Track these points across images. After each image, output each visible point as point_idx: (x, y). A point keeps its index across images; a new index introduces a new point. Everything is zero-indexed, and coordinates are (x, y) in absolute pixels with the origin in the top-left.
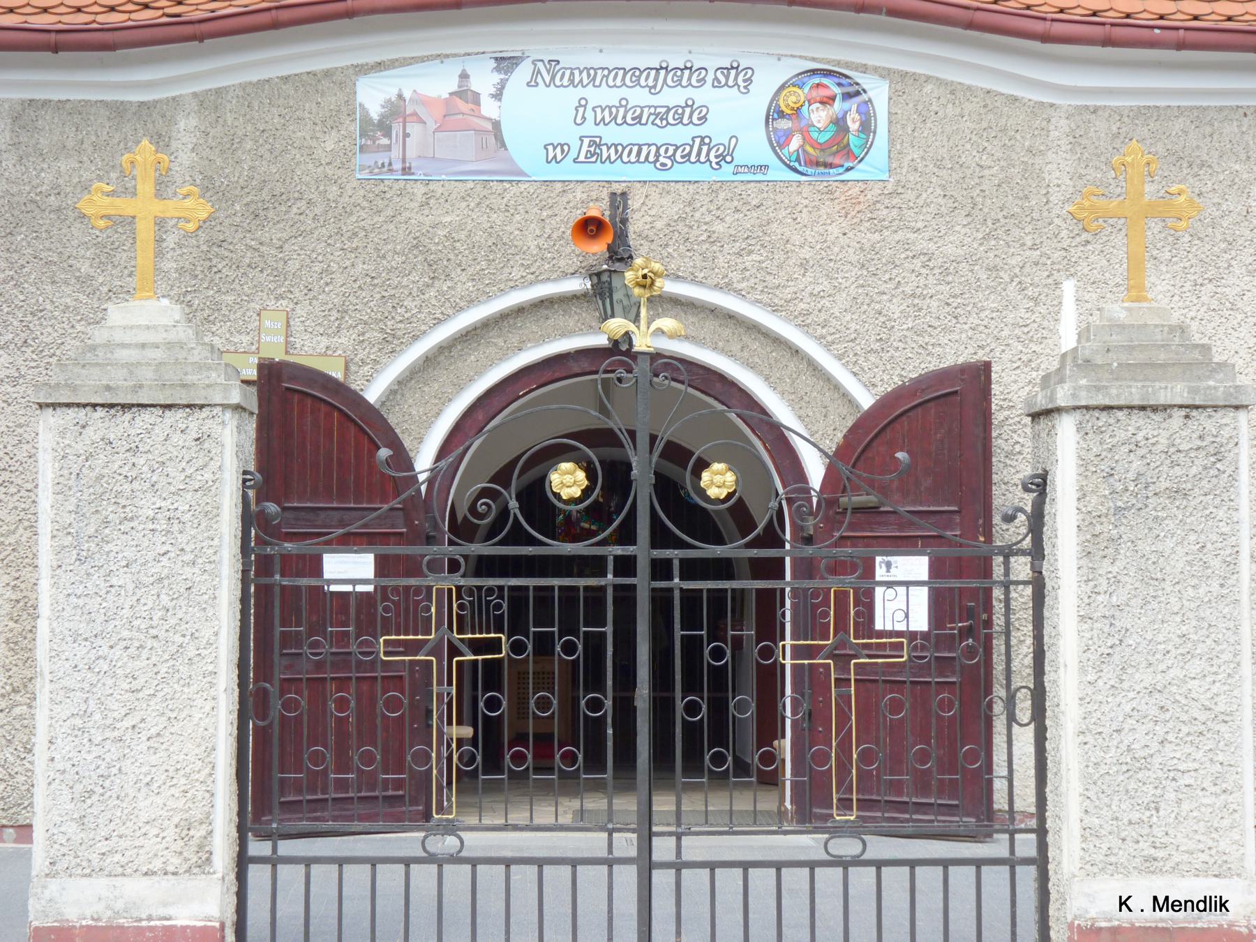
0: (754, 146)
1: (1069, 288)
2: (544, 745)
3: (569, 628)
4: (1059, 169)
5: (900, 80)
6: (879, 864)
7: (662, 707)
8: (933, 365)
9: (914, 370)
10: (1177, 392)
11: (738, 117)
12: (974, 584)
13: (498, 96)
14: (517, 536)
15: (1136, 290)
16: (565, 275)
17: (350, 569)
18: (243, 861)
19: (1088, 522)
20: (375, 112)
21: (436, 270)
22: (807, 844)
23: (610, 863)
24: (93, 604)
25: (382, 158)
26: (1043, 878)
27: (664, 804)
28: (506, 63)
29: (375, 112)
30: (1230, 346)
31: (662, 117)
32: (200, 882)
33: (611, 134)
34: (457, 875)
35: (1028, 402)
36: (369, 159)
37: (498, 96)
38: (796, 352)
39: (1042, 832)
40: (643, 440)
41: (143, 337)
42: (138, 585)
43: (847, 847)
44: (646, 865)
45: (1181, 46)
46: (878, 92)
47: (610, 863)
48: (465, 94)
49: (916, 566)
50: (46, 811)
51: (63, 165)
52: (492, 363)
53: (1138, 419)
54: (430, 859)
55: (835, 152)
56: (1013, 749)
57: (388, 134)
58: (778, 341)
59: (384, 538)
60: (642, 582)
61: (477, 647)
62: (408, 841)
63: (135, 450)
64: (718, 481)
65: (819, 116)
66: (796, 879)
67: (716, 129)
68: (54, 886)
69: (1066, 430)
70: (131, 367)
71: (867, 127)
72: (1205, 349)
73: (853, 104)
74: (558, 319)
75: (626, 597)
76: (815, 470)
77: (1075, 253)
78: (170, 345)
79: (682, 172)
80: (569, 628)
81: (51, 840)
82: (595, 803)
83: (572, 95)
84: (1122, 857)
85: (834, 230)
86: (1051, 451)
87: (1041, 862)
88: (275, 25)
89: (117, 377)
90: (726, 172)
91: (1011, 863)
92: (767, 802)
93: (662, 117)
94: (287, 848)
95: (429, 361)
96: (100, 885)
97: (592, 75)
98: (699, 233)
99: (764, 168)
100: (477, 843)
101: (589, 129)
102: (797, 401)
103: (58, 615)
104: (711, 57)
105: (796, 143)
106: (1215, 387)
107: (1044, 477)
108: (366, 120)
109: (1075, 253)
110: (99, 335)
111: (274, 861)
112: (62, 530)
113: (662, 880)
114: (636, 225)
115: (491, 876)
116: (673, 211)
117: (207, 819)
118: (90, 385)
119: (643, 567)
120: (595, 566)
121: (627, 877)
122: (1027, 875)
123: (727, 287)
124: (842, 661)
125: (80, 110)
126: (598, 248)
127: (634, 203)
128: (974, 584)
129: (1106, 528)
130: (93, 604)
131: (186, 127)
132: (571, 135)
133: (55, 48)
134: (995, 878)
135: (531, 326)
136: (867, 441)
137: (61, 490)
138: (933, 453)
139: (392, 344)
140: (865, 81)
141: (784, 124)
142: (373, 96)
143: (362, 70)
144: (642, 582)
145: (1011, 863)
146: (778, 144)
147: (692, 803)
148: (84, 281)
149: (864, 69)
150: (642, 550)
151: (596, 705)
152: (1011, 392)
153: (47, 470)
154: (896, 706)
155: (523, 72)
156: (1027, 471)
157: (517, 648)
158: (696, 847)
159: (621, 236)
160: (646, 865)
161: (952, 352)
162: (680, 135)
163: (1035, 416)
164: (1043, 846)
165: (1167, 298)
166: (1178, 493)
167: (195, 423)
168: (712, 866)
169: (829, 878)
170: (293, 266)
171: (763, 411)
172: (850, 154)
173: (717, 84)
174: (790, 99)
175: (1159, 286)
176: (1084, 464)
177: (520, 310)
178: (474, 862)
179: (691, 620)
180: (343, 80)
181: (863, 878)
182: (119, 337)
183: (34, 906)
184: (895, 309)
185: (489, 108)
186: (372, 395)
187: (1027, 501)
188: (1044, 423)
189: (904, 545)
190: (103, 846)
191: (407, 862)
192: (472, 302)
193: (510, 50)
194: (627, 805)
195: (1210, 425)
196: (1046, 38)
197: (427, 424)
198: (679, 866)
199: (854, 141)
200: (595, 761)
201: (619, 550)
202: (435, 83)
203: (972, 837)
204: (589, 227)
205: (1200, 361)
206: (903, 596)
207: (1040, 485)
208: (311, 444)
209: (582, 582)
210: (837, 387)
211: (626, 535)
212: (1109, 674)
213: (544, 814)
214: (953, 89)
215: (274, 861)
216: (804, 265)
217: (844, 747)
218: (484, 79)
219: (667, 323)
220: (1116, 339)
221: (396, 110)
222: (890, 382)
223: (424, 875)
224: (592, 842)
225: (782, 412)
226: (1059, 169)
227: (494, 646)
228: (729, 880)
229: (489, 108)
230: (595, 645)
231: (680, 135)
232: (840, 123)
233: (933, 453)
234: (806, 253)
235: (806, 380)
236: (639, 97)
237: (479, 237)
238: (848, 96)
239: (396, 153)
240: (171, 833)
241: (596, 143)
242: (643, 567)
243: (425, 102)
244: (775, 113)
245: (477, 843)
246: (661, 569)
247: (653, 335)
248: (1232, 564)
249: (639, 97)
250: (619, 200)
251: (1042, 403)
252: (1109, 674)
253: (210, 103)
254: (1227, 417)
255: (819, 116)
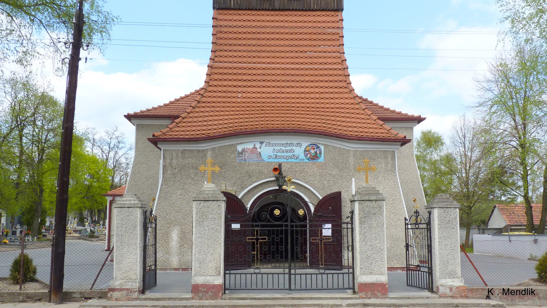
0: (302, 156)
1: (353, 179)
2: (265, 255)
3: (277, 236)
4: (351, 160)
5: (325, 146)
6: (327, 274)
7: (292, 248)
8: (332, 192)
9: (329, 192)
10: (374, 198)
11: (299, 151)
12: (339, 228)
13: (260, 148)
14: (269, 221)
15: (367, 181)
16: (271, 177)
17: (236, 226)
18: (225, 274)
19: (360, 219)
20: (240, 151)
21: (250, 177)
22: (316, 271)
23: (284, 274)
24: (202, 232)
25: (241, 158)
26: (354, 276)
27: (293, 265)
28: (261, 143)
29: (240, 151)
30: (380, 189)
31: (287, 151)
32: (219, 277)
33: (279, 154)
34: (259, 276)
35: (350, 199)
36: (239, 158)
37: (260, 148)
38: (309, 190)
39: (353, 268)
40: (289, 206)
41: (209, 189)
42: (209, 229)
43: (322, 271)
44: (290, 274)
45: (371, 141)
46: (322, 148)
47: (284, 274)
48: (255, 148)
49: (329, 226)
50: (195, 266)
51: (189, 160)
52: (259, 192)
53: (368, 202)
54: (255, 273)
55: (315, 157)
56: (346, 255)
57: (242, 154)
58: (306, 188)
59: (244, 221)
60: (289, 229)
61: (262, 239)
62: (252, 270)
63: (208, 208)
64: (301, 212)
65: (313, 151)
66: (314, 277)
67: (296, 153)
68: (196, 278)
69: (357, 204)
70: (208, 194)
71: (320, 153)
72: (378, 191)
73: (318, 150)
74: (270, 184)
75: (286, 231)
76: (313, 209)
77: (354, 174)
78: (214, 191)
79: (290, 160)
80: (277, 236)
81: (195, 270)
82: (282, 265)
83: (273, 148)
84: (366, 272)
85: (315, 170)
86: (354, 207)
87: (353, 273)
88: (224, 137)
89: (205, 196)
90: (298, 160)
91: (349, 273)
92: (305, 265)
93: (287, 151)
94: (232, 272)
95: (249, 191)
96: (203, 278)
97: (276, 145)
98: (293, 170)
99: (303, 160)
100: (263, 271)
101: (275, 153)
102: (309, 198)
103: (196, 234)
104: (295, 142)
105: (309, 156)
106: (380, 197)
107: (353, 211)
108: (239, 152)
109: (354, 174)
110: (202, 189)
111: (230, 274)
112: (197, 220)
113: (293, 276)
114: (283, 169)
115: (265, 276)
116: (289, 167)
117: (220, 267)
118: (201, 197)
119: (289, 226)
120: (282, 226)
121: (287, 276)
122: (351, 275)
123: (298, 179)
124: (321, 241)
125: (192, 151)
126: (277, 173)
127: (283, 165)
128: (339, 228)
129: (363, 219)
130: (202, 232)
131: (209, 153)
132: (272, 154)
133: (189, 141)
134: (346, 276)
135: (265, 185)
136: (323, 204)
137: (197, 214)
138: (332, 206)
139: (243, 189)
140: (320, 146)
141: (307, 153)
142: (240, 148)
143: (238, 144)
144: (289, 229)
145: (349, 273)
146: (306, 156)
147: (297, 265)
148: (192, 178)
149: (320, 144)
150: (289, 223)
151: (282, 248)
152: (345, 198)
153: (194, 211)
154: (330, 248)
155: (264, 144)
156: (350, 210)
157: (269, 239)
158: (298, 271)
159: (281, 171)
160: (290, 274)
161: (335, 190)
162: (290, 154)
163: (351, 201)
164: (353, 271)
165: (372, 183)
166: (374, 214)
167: (218, 203)
168: (301, 274)
169: (319, 276)
170: (227, 176)
171: (304, 200)
172: (318, 157)
173: (296, 146)
174: (308, 148)
175: (370, 183)
176: (359, 209)
177: (264, 183)
178: (262, 274)
179: (297, 234)
180: (235, 146)
181: (325, 276)
182: (206, 189)
183: (192, 281)
184: (325, 183)
185: (259, 150)
186: (240, 197)
187: (350, 215)
188: (353, 203)
189: (328, 222)
190: (203, 271)
191: (251, 274)
192: (256, 182)
193: (262, 141)
194: (287, 265)
195: (379, 203)
196: (349, 139)
197: (249, 202)
198: (295, 274)
199: (318, 155)
200: (282, 257)
201: (285, 223)
202: (250, 146)
203: (339, 270)
204: (275, 170)
205: (377, 193)
206: (327, 230)
207: (352, 212)
208: (234, 205)
209: (279, 228)
210: (316, 195)
211: (286, 221)
212: (364, 243)
213: (269, 266)
214: (334, 147)
215: (230, 274)
216: (310, 175)
217: (322, 255)
218: (258, 146)
219: (293, 187)
220: (364, 189)
221: (243, 150)
222: (325, 195)
223: (254, 276)
224: (280, 271)
225: (307, 199)
226: (351, 160)
227: (265, 239)
228: (303, 277)
229: (259, 150)
230: (282, 238)
231: (290, 154)
232: (316, 152)
233: (332, 206)
234: (311, 174)
235: (311, 194)
236: (283, 148)
237: (257, 171)
238: (317, 148)
239: (243, 157)
240: (214, 269)
241: (276, 156)
242: (289, 226)
243: (248, 149)
244: (305, 151)
245: (263, 271)
246: (292, 226)
247: (290, 188)
248: (383, 225)
249: (283, 148)
250: (280, 165)
251: (352, 199)
252: (364, 243)
253: (213, 149)
254: (382, 202)
255: (313, 151)
